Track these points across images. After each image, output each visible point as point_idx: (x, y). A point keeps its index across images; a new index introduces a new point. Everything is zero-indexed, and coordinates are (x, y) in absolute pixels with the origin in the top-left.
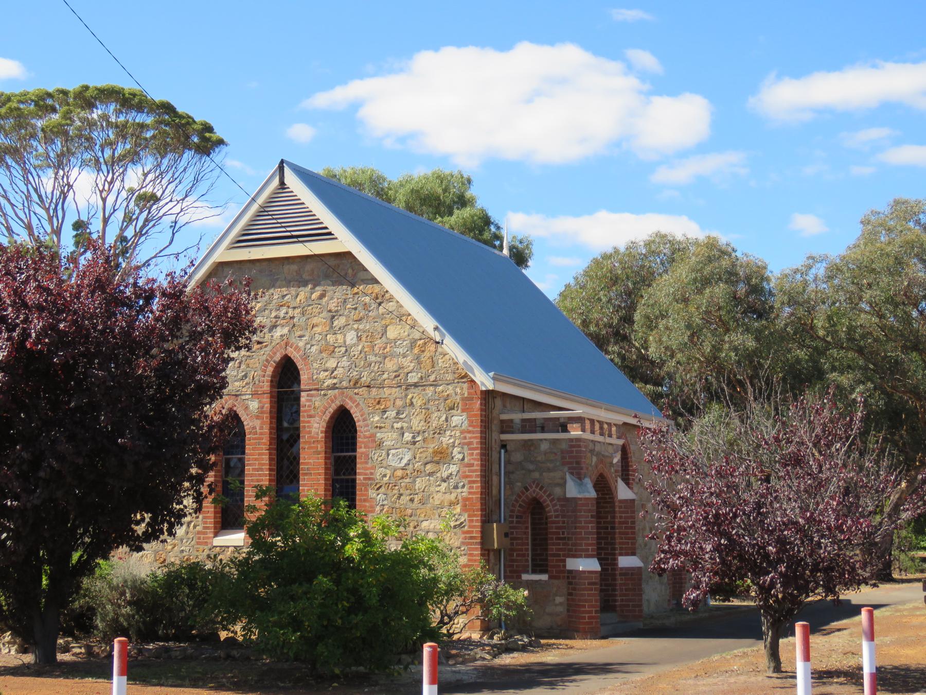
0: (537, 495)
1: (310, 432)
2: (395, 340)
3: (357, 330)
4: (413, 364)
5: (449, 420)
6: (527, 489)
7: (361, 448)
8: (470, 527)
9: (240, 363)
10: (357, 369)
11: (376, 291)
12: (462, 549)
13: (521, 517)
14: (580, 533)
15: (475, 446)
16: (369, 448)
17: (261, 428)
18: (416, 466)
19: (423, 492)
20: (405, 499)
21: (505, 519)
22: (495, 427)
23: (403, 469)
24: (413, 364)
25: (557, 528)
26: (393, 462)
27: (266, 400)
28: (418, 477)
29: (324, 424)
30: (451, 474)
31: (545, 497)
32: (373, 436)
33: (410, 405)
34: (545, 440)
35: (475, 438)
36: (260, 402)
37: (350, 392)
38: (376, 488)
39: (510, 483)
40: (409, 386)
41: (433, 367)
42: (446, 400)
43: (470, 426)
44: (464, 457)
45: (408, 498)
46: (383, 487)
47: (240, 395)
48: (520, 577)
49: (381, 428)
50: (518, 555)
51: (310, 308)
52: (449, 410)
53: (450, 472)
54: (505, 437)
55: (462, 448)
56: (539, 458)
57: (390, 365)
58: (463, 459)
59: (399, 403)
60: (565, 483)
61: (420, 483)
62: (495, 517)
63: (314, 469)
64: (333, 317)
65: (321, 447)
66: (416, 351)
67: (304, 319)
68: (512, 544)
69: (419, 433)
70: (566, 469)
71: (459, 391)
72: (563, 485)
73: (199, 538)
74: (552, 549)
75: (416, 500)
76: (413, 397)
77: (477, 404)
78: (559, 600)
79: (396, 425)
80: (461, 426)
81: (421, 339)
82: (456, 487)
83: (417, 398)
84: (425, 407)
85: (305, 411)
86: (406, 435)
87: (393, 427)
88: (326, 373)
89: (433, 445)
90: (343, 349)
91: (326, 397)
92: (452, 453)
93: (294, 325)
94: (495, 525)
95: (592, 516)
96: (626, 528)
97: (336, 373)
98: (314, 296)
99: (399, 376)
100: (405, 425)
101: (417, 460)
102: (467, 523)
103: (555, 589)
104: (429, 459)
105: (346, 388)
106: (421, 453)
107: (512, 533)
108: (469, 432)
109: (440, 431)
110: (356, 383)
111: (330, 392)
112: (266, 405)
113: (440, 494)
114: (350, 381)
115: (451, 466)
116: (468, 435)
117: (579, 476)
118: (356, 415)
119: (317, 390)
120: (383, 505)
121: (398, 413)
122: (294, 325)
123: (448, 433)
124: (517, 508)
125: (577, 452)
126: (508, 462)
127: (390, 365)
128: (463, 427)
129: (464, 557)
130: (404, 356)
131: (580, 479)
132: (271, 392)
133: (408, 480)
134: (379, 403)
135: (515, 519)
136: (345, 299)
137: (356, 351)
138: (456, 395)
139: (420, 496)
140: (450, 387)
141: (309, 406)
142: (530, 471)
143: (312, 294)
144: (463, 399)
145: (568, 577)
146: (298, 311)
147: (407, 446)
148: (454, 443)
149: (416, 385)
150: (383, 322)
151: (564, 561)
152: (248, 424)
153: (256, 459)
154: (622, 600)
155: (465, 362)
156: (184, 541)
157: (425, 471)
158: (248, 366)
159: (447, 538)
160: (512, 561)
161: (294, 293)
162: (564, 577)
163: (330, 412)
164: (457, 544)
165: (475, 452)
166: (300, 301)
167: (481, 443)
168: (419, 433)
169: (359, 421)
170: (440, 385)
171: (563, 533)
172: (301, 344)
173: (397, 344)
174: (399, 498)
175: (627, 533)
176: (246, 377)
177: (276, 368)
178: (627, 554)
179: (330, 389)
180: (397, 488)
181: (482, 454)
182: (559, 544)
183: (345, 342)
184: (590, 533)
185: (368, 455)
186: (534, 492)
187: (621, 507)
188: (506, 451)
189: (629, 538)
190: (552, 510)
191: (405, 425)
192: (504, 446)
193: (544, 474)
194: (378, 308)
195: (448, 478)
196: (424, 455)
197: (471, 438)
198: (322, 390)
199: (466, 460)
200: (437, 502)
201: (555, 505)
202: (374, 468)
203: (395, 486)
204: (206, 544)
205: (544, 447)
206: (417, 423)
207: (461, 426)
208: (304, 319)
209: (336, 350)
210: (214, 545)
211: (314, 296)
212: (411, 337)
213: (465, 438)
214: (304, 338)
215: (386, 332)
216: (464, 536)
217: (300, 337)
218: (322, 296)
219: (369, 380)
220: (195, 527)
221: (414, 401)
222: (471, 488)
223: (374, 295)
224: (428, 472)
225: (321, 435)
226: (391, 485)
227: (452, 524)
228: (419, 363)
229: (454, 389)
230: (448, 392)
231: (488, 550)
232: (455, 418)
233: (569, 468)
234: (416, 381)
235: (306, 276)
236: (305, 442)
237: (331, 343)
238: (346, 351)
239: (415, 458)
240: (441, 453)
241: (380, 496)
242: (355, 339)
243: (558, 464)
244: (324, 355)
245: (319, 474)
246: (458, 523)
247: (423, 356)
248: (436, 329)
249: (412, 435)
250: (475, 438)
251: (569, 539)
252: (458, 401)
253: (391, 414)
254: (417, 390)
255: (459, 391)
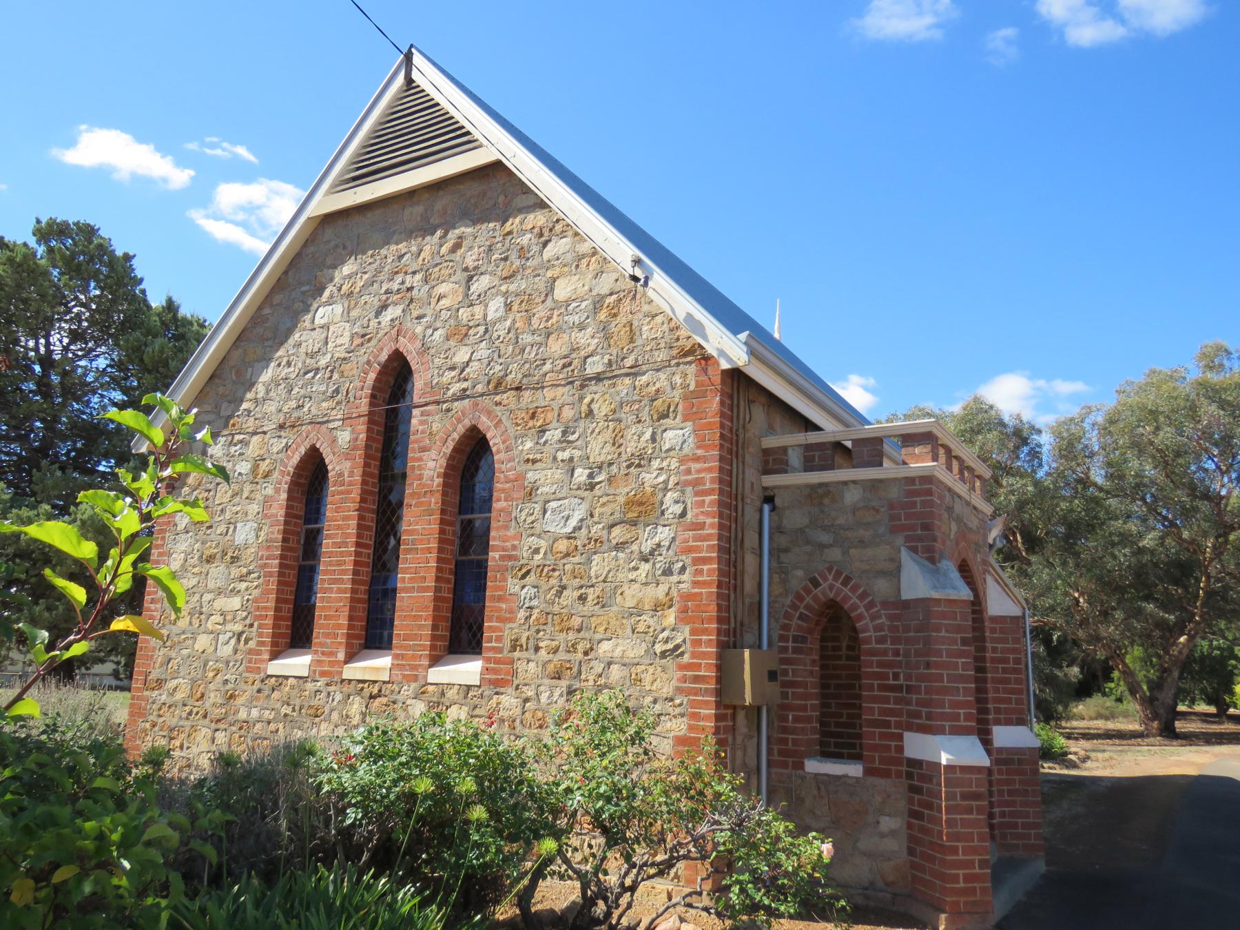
0: (837, 594)
1: (420, 477)
2: (567, 303)
3: (506, 294)
4: (596, 340)
5: (658, 440)
6: (816, 584)
7: (499, 500)
8: (694, 655)
9: (332, 371)
10: (501, 361)
11: (540, 223)
12: (677, 702)
13: (803, 640)
14: (939, 678)
15: (708, 486)
16: (512, 500)
17: (351, 474)
18: (593, 530)
19: (604, 581)
20: (570, 595)
21: (770, 644)
22: (752, 459)
23: (569, 538)
24: (596, 340)
25: (881, 664)
26: (554, 525)
27: (362, 427)
28: (595, 553)
29: (443, 462)
30: (659, 545)
31: (854, 600)
32: (521, 477)
33: (587, 416)
34: (854, 482)
35: (709, 470)
36: (353, 432)
37: (486, 401)
38: (520, 574)
39: (780, 571)
40: (586, 381)
41: (632, 340)
42: (653, 401)
43: (698, 447)
44: (685, 509)
45: (576, 594)
46: (532, 573)
47: (328, 422)
48: (801, 766)
49: (534, 461)
50: (796, 719)
51: (437, 269)
52: (659, 420)
53: (657, 540)
54: (771, 480)
55: (683, 492)
56: (841, 521)
57: (556, 347)
58: (683, 514)
59: (568, 413)
60: (899, 569)
61: (599, 565)
62: (749, 638)
63: (421, 541)
64: (471, 278)
65: (435, 501)
66: (602, 316)
67: (427, 288)
68: (784, 695)
69: (600, 468)
70: (900, 540)
71: (679, 381)
72: (895, 573)
73: (250, 661)
74: (872, 710)
75: (590, 598)
76: (592, 401)
77: (714, 403)
78: (888, 823)
79: (561, 456)
80: (681, 449)
81: (611, 294)
82: (668, 572)
83: (601, 401)
84: (614, 417)
85: (417, 441)
86: (578, 471)
87: (555, 458)
88: (453, 373)
89: (626, 490)
90: (482, 329)
91: (450, 414)
92: (662, 503)
93: (412, 301)
94: (747, 653)
95: (965, 642)
96: (1005, 671)
97: (468, 370)
98: (444, 250)
99: (570, 364)
100: (577, 453)
101: (596, 519)
102: (687, 647)
103: (879, 799)
104: (617, 516)
105: (482, 395)
106: (604, 505)
107: (785, 672)
108: (697, 459)
109: (640, 461)
110: (499, 384)
111: (456, 404)
112: (361, 436)
113: (637, 586)
114: (489, 382)
115: (660, 529)
116: (695, 466)
117: (930, 556)
118: (495, 441)
119: (438, 403)
120: (530, 608)
121: (564, 433)
122: (412, 301)
123: (656, 464)
124: (795, 622)
125: (924, 503)
126: (777, 530)
127: (556, 347)
128: (686, 450)
129: (680, 720)
130: (582, 327)
131: (932, 560)
132: (371, 413)
133: (577, 559)
134: (533, 416)
135: (790, 644)
136: (490, 246)
137: (501, 330)
138: (673, 389)
139: (598, 590)
140: (662, 375)
141: (423, 432)
142: (822, 547)
143: (441, 246)
144: (685, 397)
145: (910, 776)
146: (418, 277)
147: (579, 492)
148: (666, 482)
149: (598, 378)
150: (549, 274)
151: (900, 737)
152: (333, 469)
153: (339, 527)
154: (1003, 814)
155: (689, 316)
156: (231, 664)
157: (609, 541)
158: (342, 375)
159: (647, 678)
160: (785, 730)
161: (414, 249)
162: (899, 774)
163: (453, 440)
164: (667, 690)
165: (708, 499)
166: (424, 260)
167: (721, 481)
168: (600, 468)
169: (499, 452)
170: (644, 374)
171: (896, 677)
172: (419, 329)
173: (570, 308)
174: (559, 594)
175: (1007, 681)
176: (338, 393)
177: (380, 373)
178: (1008, 722)
179: (457, 400)
180: (557, 573)
181: (721, 503)
182: (886, 700)
183: (485, 316)
184: (962, 679)
185: (510, 513)
186: (829, 588)
187: (993, 630)
188: (773, 509)
189: (1012, 692)
190: (869, 629)
191: (577, 453)
192: (769, 499)
193: (852, 551)
194: (541, 252)
195: (652, 553)
196: (608, 509)
197: (699, 471)
198: (444, 402)
199: (689, 515)
200: (630, 603)
201: (874, 617)
202: (519, 536)
203: (554, 570)
204: (258, 670)
205: (852, 497)
206: (599, 449)
207: (681, 449)
208: (427, 288)
209: (472, 332)
210: (269, 673)
211: (444, 250)
212: (594, 293)
213: (688, 472)
214: (425, 320)
215: (552, 289)
216: (680, 674)
217: (419, 318)
218: (456, 247)
219: (520, 376)
220: (246, 642)
221: (595, 406)
222: (699, 572)
223: (536, 230)
224: (614, 542)
225: (438, 481)
226: (546, 570)
227: (659, 648)
228: (607, 338)
229: (669, 380)
230: (658, 385)
231: (735, 707)
232: (669, 434)
233: (908, 539)
234: (599, 370)
235: (435, 220)
236: (413, 495)
237: (465, 322)
238: (486, 331)
239: (592, 516)
240: (641, 504)
241: (525, 590)
242: (502, 309)
243: (882, 530)
244: (452, 343)
245: (429, 550)
246: (670, 646)
247: (613, 325)
248: (637, 262)
249: (587, 471)
250: (709, 470)
251: (909, 689)
252: (677, 400)
253: (554, 434)
254: (600, 388)
255: (679, 381)
